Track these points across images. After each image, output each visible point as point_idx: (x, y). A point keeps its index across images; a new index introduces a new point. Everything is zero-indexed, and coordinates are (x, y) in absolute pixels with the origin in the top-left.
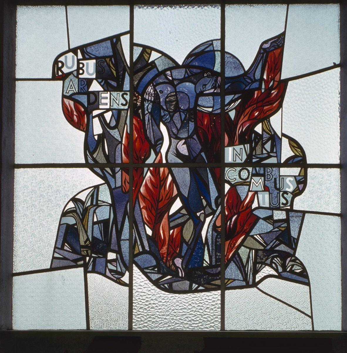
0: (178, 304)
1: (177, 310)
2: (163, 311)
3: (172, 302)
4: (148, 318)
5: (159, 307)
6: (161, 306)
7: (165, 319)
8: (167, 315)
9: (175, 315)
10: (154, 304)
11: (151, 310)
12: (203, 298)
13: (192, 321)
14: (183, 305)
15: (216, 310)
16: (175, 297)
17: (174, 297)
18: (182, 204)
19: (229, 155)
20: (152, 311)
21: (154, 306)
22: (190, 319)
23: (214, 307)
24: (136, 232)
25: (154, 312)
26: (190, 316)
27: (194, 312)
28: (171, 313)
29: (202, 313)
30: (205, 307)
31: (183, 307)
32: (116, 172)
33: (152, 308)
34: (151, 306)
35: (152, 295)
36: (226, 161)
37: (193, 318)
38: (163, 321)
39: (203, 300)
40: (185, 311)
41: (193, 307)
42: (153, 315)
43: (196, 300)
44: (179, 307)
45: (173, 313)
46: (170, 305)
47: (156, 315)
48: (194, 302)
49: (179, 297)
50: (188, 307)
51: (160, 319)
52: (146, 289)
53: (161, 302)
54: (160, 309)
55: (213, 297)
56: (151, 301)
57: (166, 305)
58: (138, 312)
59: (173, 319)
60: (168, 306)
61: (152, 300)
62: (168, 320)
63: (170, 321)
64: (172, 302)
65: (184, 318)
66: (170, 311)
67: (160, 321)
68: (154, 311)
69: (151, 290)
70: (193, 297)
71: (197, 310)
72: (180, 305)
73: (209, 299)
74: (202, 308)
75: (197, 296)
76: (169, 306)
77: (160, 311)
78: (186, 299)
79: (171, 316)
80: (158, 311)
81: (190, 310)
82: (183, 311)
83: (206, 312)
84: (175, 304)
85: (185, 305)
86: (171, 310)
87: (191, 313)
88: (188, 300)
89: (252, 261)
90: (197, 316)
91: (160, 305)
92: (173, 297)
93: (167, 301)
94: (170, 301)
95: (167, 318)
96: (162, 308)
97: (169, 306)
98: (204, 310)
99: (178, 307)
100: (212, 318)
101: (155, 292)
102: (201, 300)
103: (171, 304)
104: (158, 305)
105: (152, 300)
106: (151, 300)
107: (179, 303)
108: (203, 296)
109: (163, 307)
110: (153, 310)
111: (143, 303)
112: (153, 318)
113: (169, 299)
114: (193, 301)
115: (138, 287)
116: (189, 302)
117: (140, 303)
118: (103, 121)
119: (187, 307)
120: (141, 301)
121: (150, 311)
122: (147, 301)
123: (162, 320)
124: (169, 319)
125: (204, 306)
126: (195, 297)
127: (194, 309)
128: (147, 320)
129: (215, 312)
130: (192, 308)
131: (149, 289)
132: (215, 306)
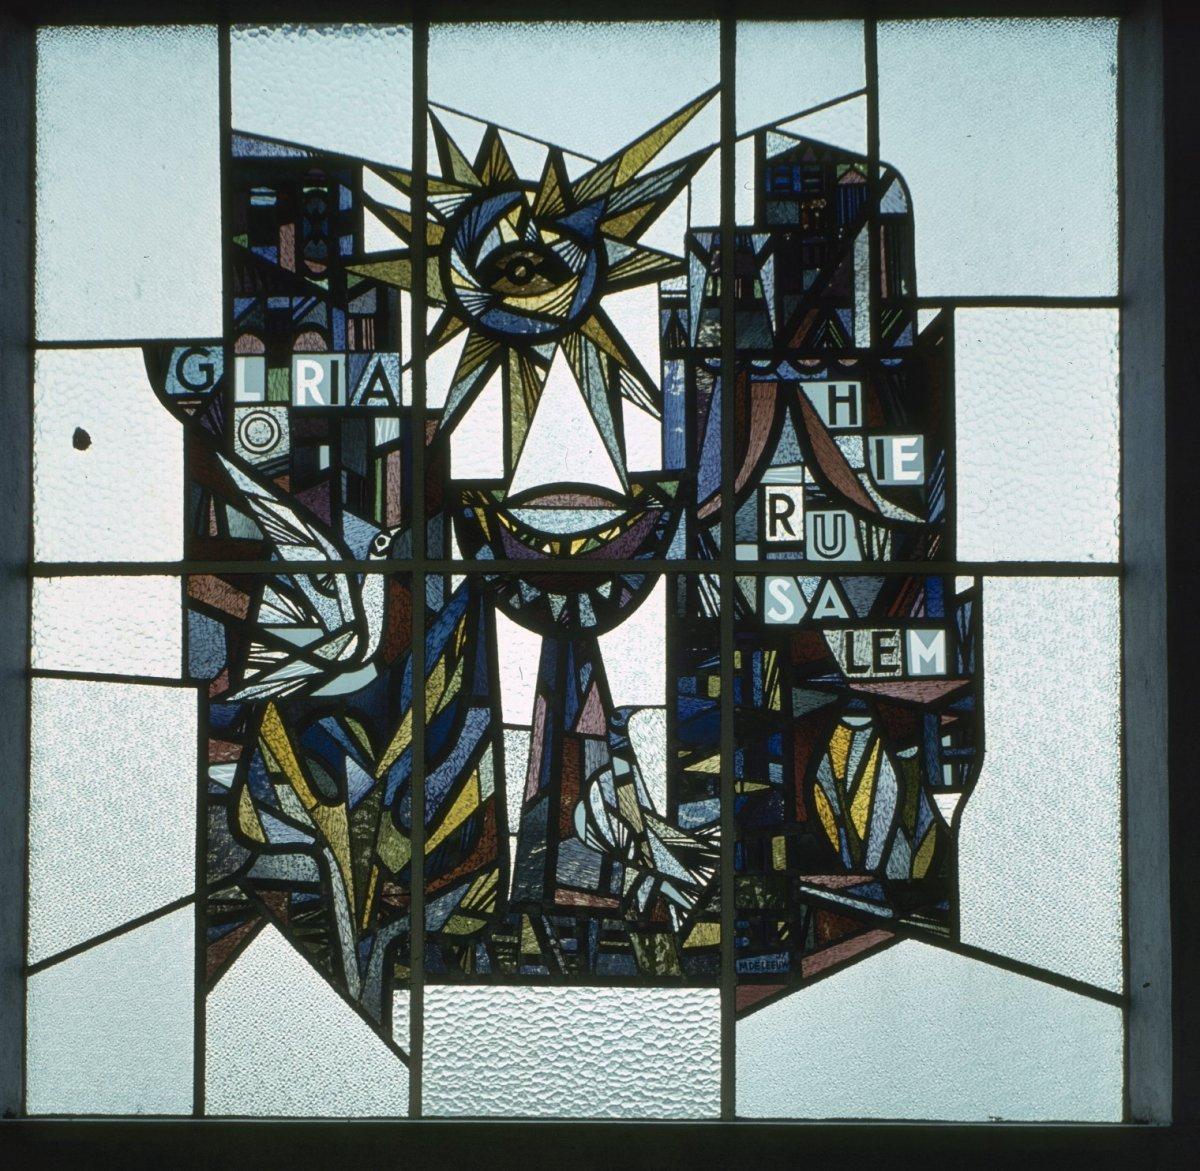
0: (454, 1050)
1: (704, 1072)
2: (657, 1077)
3: (690, 1047)
4: (610, 1096)
5: (647, 1065)
6: (653, 1059)
7: (667, 1101)
8: (672, 1089)
9: (446, 1087)
10: (628, 1051)
11: (619, 1072)
12: (577, 1032)
13: (539, 1107)
14: (513, 1053)
15: (614, 1074)
16: (698, 1031)
17: (696, 1032)
18: (596, 641)
19: (403, 325)
20: (622, 1076)
21: (629, 1058)
22: (533, 1100)
23: (607, 1062)
24: (294, 689)
25: (628, 1079)
26: (535, 1090)
27: (547, 1079)
28: (433, 1081)
29: (572, 1081)
30: (579, 1062)
31: (512, 1060)
32: (334, 310)
33: (621, 1066)
34: (620, 1060)
35: (626, 1024)
36: (288, 306)
37: (542, 1097)
38: (660, 1107)
39: (574, 1038)
40: (516, 1073)
41: (543, 1060)
42: (626, 1089)
43: (554, 1038)
44: (712, 1065)
45: (694, 1083)
46: (681, 1056)
47: (638, 1089)
48: (546, 1046)
49: (457, 1028)
50: (528, 1059)
51: (651, 1103)
52: (607, 1002)
53: (651, 1045)
54: (646, 1070)
55: (606, 1029)
56: (621, 1043)
57: (670, 1055)
58: (577, 1080)
59: (693, 1102)
60: (677, 1061)
61: (623, 1038)
62: (678, 1106)
63: (683, 1108)
64: (690, 1047)
65: (515, 1095)
66: (681, 1076)
67: (648, 1107)
68: (627, 1076)
69: (623, 1007)
70: (543, 1030)
71: (554, 1072)
72: (502, 1055)
73: (595, 1037)
74: (571, 1064)
75: (557, 1026)
76: (682, 1060)
77: (647, 1076)
78: (523, 1034)
79: (685, 1094)
80: (641, 1078)
81: (533, 1072)
82: (512, 1076)
83: (583, 1077)
84: (486, 1050)
85: (518, 1055)
86: (431, 1071)
87: (535, 1080)
88: (528, 1039)
89: (471, 895)
90: (555, 1091)
91: (648, 1058)
92: (693, 1029)
93: (674, 1043)
94: (683, 1045)
95: (672, 1098)
96: (656, 1066)
97: (682, 1060)
98: (577, 1072)
99: (709, 1063)
100: (602, 1097)
101: (637, 1013)
102: (567, 1039)
103: (685, 1054)
104: (642, 1058)
105: (623, 1038)
106: (620, 1039)
107: (500, 1048)
108: (575, 1026)
109: (659, 1063)
110: (625, 1072)
111: (594, 1048)
112: (625, 1097)
113: (679, 1038)
114: (542, 1043)
115: (580, 997)
116: (530, 1045)
117: (586, 1049)
118: (882, 244)
119: (524, 1061)
120: (587, 1044)
121: (616, 1075)
122: (608, 1043)
123: (653, 1106)
124: (679, 1102)
125: (578, 1058)
126: (551, 1029)
127: (545, 1069)
128: (608, 1105)
129: (613, 1081)
130: (539, 1064)
131: (616, 1003)
132: (613, 1059)
